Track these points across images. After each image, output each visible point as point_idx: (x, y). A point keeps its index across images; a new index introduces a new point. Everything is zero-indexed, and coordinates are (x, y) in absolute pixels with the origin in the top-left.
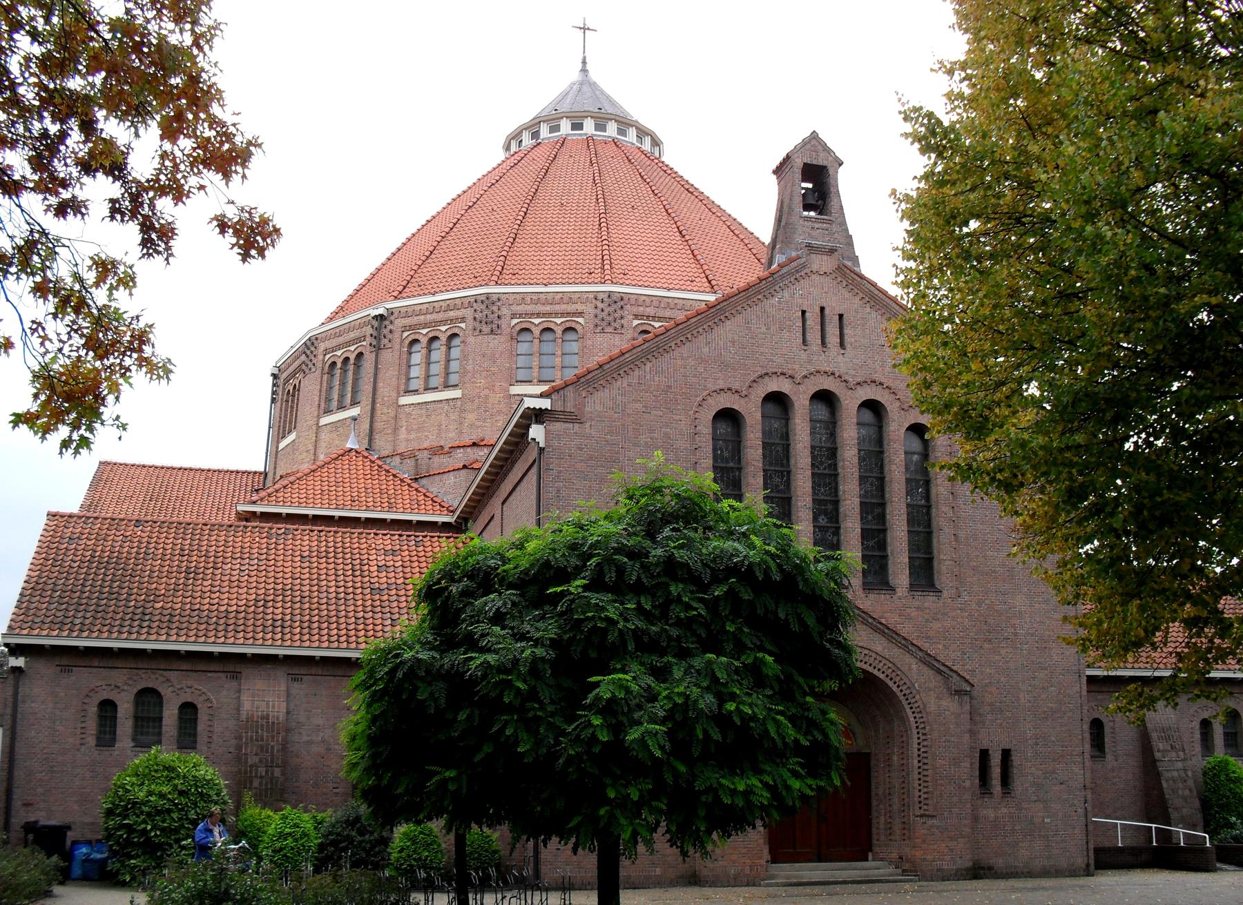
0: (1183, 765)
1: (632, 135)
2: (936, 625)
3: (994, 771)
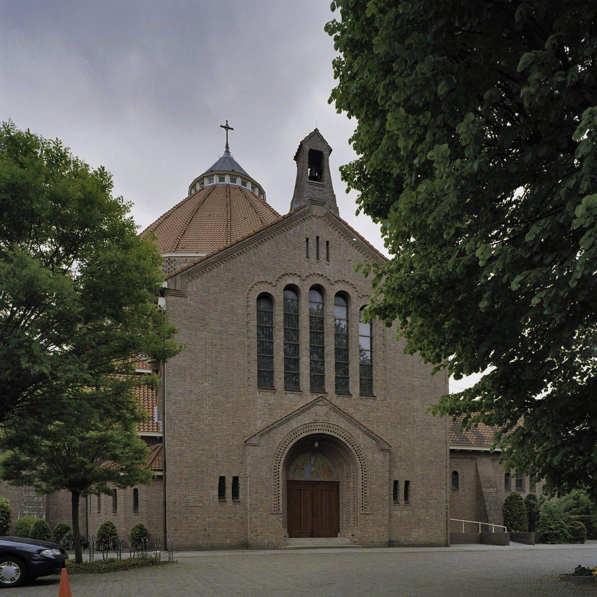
0: (497, 494)
1: (249, 186)
2: (373, 415)
3: (400, 491)
